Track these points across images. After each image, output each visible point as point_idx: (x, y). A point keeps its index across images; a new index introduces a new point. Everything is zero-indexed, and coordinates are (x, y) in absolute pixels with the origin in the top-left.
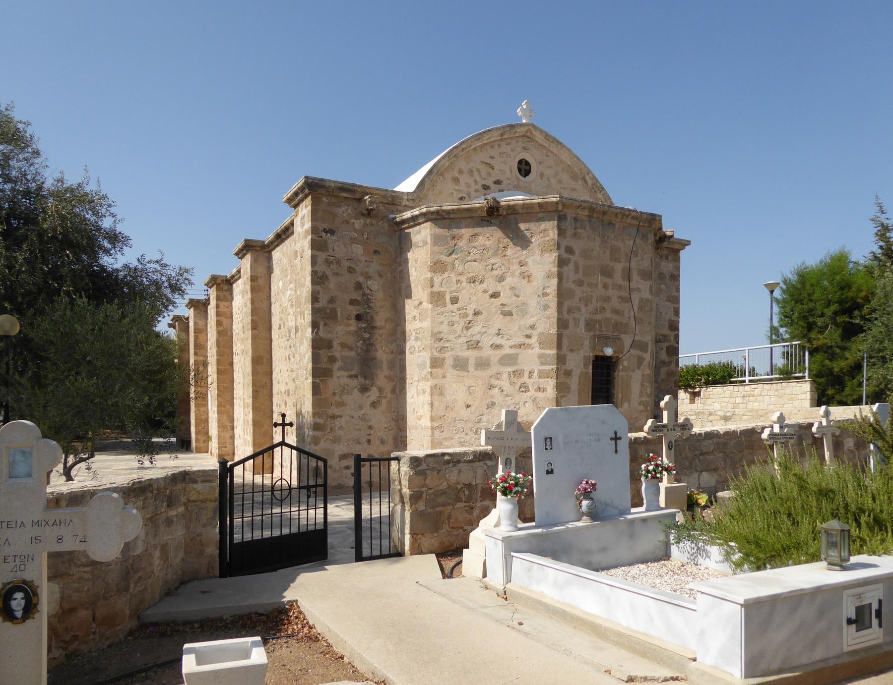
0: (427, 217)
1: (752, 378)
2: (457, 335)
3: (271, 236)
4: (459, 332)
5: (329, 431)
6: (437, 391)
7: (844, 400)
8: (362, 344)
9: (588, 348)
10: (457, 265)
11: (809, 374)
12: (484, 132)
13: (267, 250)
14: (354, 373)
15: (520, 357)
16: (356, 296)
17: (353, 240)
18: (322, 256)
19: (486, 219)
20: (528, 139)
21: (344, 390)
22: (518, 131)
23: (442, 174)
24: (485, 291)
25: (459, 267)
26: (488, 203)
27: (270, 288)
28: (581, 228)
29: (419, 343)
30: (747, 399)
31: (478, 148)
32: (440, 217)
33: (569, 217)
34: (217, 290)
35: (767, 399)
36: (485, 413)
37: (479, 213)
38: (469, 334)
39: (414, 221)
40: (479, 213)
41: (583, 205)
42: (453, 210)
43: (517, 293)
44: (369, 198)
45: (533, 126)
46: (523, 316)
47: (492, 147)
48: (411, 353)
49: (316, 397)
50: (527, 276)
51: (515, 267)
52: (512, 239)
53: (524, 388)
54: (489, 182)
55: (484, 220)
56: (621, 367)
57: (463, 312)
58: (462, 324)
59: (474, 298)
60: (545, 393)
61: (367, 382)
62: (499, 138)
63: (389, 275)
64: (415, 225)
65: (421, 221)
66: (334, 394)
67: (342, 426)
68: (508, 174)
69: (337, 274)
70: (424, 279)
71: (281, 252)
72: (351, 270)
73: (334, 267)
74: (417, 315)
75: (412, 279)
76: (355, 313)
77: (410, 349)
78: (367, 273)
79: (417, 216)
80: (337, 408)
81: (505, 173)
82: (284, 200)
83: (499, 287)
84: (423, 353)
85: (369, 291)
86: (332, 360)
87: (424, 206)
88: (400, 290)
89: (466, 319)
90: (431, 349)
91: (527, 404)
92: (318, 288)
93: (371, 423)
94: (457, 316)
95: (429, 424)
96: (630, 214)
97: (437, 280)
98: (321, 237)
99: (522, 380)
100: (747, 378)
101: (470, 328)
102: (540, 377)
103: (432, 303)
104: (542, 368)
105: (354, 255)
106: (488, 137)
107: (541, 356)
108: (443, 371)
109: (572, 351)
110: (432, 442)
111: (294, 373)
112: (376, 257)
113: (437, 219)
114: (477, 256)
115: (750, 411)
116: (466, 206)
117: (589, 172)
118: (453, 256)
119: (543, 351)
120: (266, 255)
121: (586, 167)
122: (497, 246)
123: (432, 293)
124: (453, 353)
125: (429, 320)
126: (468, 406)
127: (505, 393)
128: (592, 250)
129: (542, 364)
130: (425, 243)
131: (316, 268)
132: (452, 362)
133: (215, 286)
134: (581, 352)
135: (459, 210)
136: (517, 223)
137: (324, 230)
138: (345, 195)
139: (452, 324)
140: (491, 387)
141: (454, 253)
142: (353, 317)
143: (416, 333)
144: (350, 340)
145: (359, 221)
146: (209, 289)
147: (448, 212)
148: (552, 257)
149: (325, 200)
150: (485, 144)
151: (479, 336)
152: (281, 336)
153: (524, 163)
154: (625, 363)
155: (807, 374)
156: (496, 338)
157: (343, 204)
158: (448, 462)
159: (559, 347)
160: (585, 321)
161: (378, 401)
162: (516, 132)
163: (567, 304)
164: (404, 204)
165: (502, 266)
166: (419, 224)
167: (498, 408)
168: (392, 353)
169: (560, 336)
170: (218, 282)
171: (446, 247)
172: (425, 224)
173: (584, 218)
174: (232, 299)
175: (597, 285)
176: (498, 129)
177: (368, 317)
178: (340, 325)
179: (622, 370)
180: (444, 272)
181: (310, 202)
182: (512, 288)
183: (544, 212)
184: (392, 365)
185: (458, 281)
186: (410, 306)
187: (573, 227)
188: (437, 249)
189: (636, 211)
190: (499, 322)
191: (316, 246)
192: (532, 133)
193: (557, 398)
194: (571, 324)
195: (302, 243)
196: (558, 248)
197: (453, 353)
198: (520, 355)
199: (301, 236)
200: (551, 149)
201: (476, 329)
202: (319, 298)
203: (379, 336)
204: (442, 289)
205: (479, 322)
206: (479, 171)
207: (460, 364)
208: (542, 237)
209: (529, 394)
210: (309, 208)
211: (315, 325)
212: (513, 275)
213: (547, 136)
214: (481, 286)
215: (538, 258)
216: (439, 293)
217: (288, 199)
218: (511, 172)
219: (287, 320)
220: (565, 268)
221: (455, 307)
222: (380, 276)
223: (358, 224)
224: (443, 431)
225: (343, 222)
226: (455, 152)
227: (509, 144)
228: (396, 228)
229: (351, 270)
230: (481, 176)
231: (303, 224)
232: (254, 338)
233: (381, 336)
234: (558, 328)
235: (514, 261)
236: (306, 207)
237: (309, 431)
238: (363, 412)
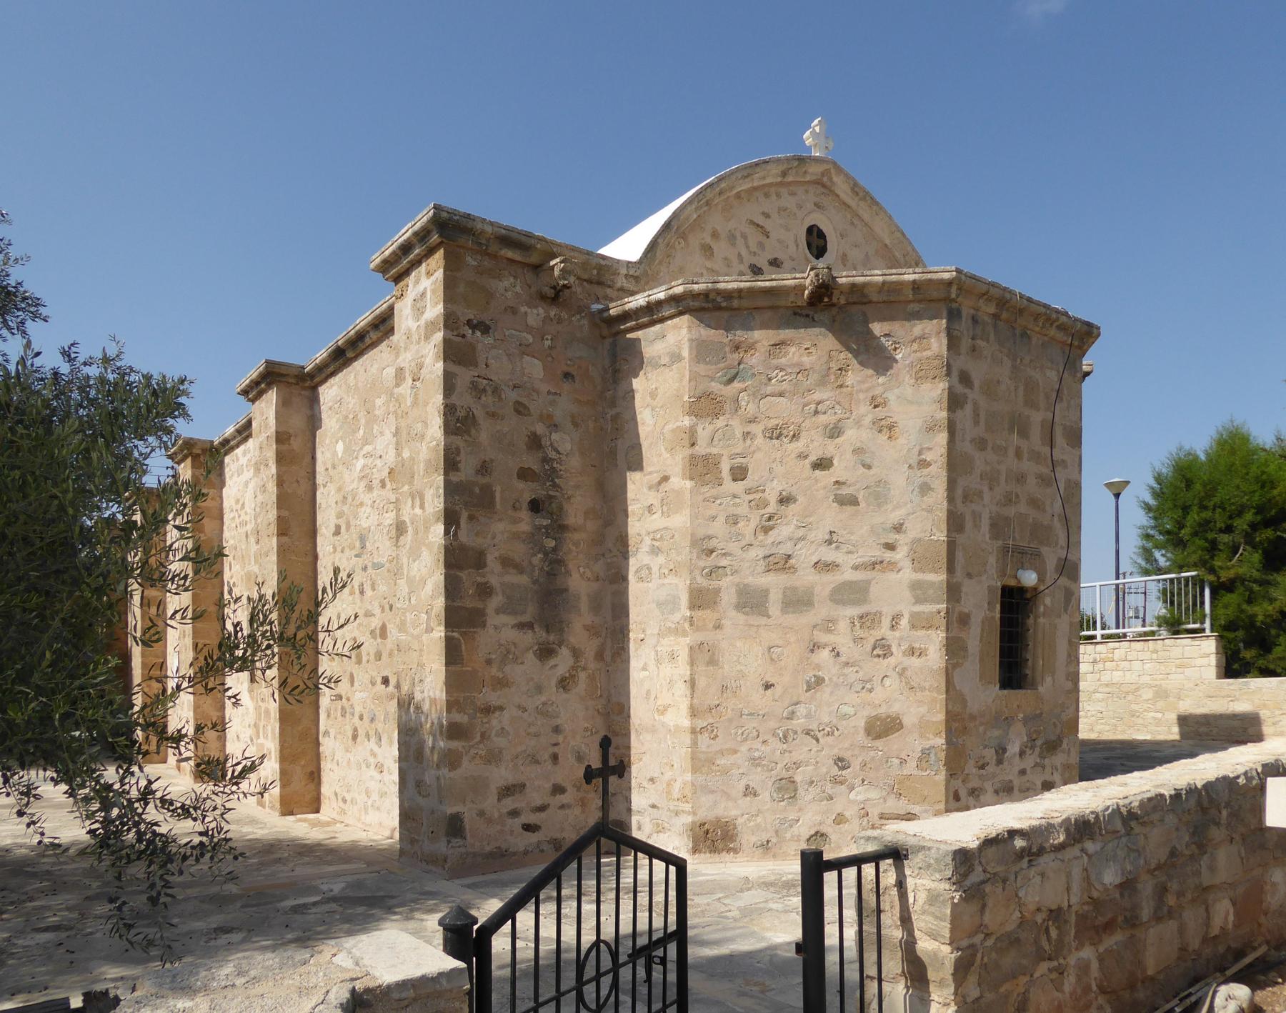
0: (682, 305)
1: (1107, 632)
2: (744, 543)
3: (321, 355)
4: (749, 537)
5: (478, 738)
6: (703, 655)
7: (1272, 667)
8: (541, 560)
9: (994, 571)
10: (743, 403)
11: (1212, 625)
12: (757, 164)
13: (307, 384)
14: (526, 618)
15: (874, 589)
16: (531, 461)
17: (525, 350)
18: (465, 376)
19: (804, 312)
20: (823, 190)
21: (509, 655)
22: (811, 170)
23: (684, 236)
24: (802, 456)
25: (748, 406)
26: (817, 275)
27: (314, 458)
28: (982, 339)
29: (661, 559)
30: (1101, 666)
31: (743, 195)
32: (710, 305)
33: (964, 313)
34: (193, 467)
35: (1137, 665)
36: (802, 699)
37: (792, 298)
38: (770, 540)
39: (652, 313)
40: (792, 298)
41: (993, 291)
42: (740, 291)
43: (868, 461)
44: (561, 262)
45: (835, 164)
46: (879, 506)
47: (767, 195)
48: (641, 579)
49: (452, 668)
50: (887, 428)
51: (864, 409)
52: (856, 354)
53: (882, 649)
54: (762, 262)
55: (800, 315)
56: (1042, 609)
57: (757, 496)
58: (754, 522)
59: (779, 469)
60: (923, 659)
61: (552, 638)
62: (779, 179)
63: (591, 424)
64: (652, 323)
65: (667, 314)
66: (489, 662)
67: (503, 728)
68: (792, 248)
69: (493, 415)
70: (673, 431)
71: (340, 387)
72: (520, 409)
73: (488, 399)
74: (656, 503)
75: (643, 431)
76: (527, 497)
77: (637, 571)
78: (550, 416)
79: (659, 303)
80: (493, 690)
81: (787, 247)
82: (372, 266)
83: (830, 448)
84: (672, 580)
85: (554, 453)
86: (485, 591)
87: (680, 282)
88: (613, 453)
89: (763, 512)
90: (691, 572)
91: (887, 682)
92: (458, 441)
93: (559, 721)
94: (746, 505)
95: (686, 723)
96: (1058, 319)
97: (704, 431)
98: (464, 336)
99: (877, 634)
100: (1099, 632)
101: (771, 528)
102: (913, 627)
103: (692, 479)
104: (918, 608)
105: (526, 379)
106: (761, 174)
107: (915, 586)
108: (715, 615)
109: (969, 575)
110: (692, 759)
111: (372, 619)
112: (566, 386)
113: (703, 309)
114: (785, 385)
115: (1107, 685)
116: (767, 284)
118: (737, 385)
119: (920, 576)
120: (306, 393)
121: (914, 250)
122: (825, 367)
123: (692, 457)
124: (736, 578)
125: (687, 512)
126: (768, 686)
127: (843, 659)
128: (998, 382)
129: (918, 601)
130: (676, 358)
131: (454, 399)
132: (735, 596)
133: (189, 461)
134: (984, 578)
135: (752, 292)
136: (866, 322)
137: (469, 322)
138: (509, 254)
139: (733, 520)
140: (815, 647)
141: (738, 379)
142: (525, 505)
143: (653, 539)
144: (519, 551)
145: (535, 311)
146: (175, 466)
147: (728, 295)
148: (937, 389)
149: (470, 261)
150: (755, 189)
151: (790, 544)
152: (339, 549)
153: (815, 234)
154: (1048, 601)
155: (1207, 625)
156: (824, 549)
157: (506, 273)
158: (1022, 854)
159: (951, 569)
160: (991, 518)
161: (572, 676)
162: (805, 172)
163: (962, 483)
164: (619, 285)
165: (837, 407)
166: (662, 320)
167: (828, 690)
168: (597, 579)
169: (951, 546)
170: (197, 451)
171: (722, 365)
172: (676, 320)
173: (986, 318)
174: (223, 484)
175: (1006, 449)
176: (778, 160)
177: (554, 505)
178: (500, 520)
179: (1044, 614)
180: (716, 415)
181: (442, 263)
182: (858, 451)
183: (920, 301)
184: (596, 606)
185: (746, 435)
186: (637, 487)
187: (971, 334)
188: (702, 369)
189: (1066, 314)
190: (830, 517)
191: (455, 354)
192: (831, 179)
193: (947, 668)
194: (969, 524)
195: (418, 351)
196: (948, 374)
197: (736, 578)
198: (873, 582)
199: (415, 337)
200: (861, 212)
201: (784, 531)
202: (460, 462)
203: (574, 544)
204: (714, 451)
205: (790, 517)
206: (744, 237)
207: (752, 602)
208: (915, 352)
209: (891, 661)
210: (439, 274)
211: (450, 518)
212: (858, 423)
213: (855, 188)
214: (794, 445)
215: (909, 391)
216: (706, 458)
217: (385, 262)
218: (797, 246)
219: (356, 516)
220: (959, 413)
221: (741, 485)
222: (576, 425)
223: (535, 315)
224: (717, 736)
225: (506, 309)
226: (709, 195)
227: (793, 194)
228: (605, 332)
229: (520, 409)
230: (748, 247)
231: (418, 311)
232: (282, 552)
233: (577, 544)
234: (948, 530)
235: (862, 396)
236: (429, 274)
237: (434, 740)
238: (543, 699)
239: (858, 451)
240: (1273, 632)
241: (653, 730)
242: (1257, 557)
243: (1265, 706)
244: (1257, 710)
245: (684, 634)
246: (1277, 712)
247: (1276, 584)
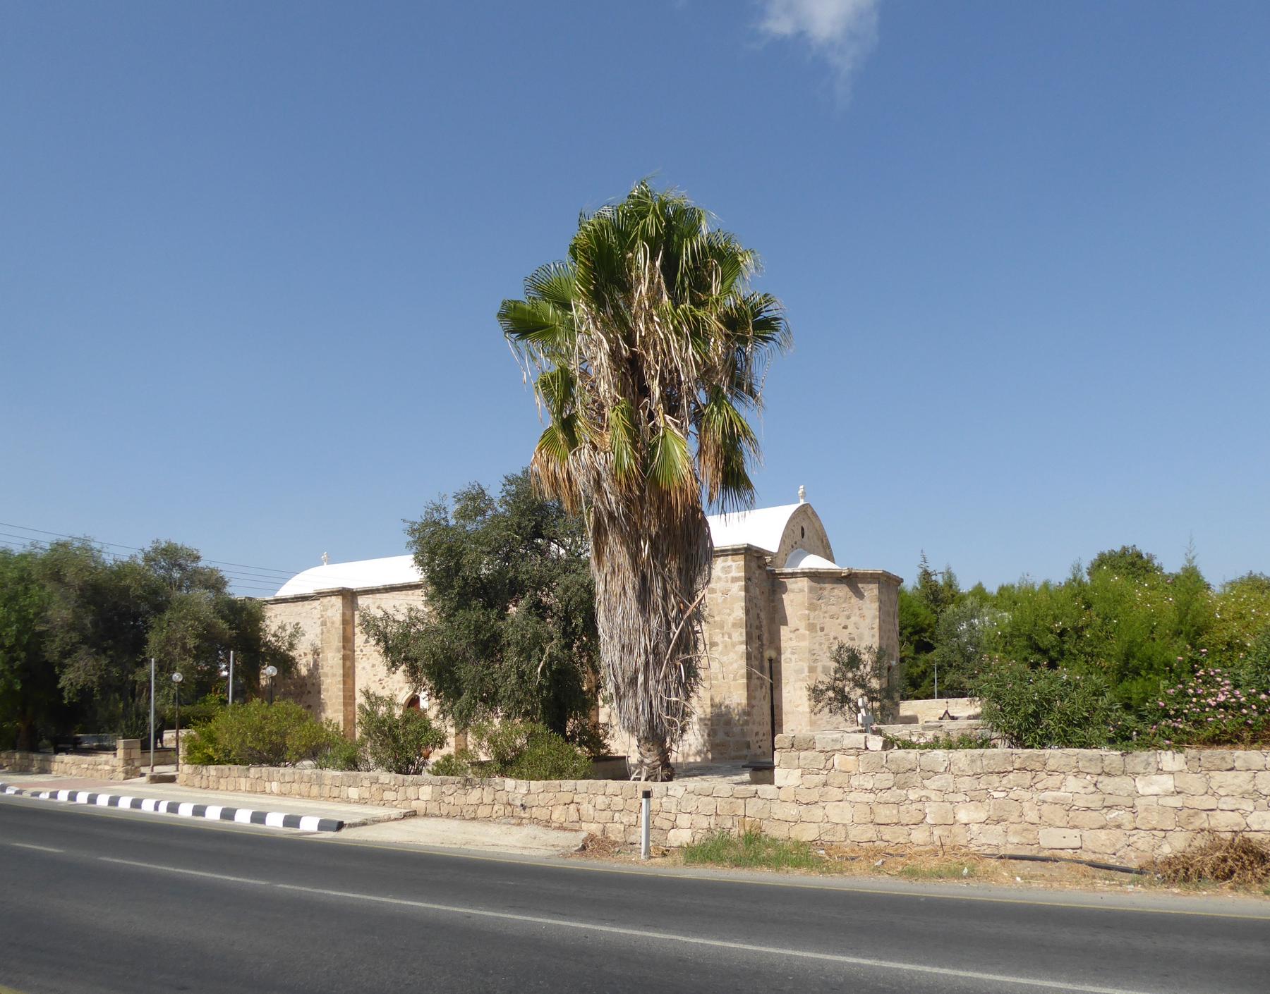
29: (796, 656)
50: (862, 616)
83: (847, 622)
117: (826, 536)
139: (821, 644)
148: (876, 605)
180: (816, 610)
185: (824, 617)
186: (784, 631)
204: (815, 622)
212: (855, 615)
239: (855, 624)
240: (919, 680)
242: (912, 648)
245: (806, 681)
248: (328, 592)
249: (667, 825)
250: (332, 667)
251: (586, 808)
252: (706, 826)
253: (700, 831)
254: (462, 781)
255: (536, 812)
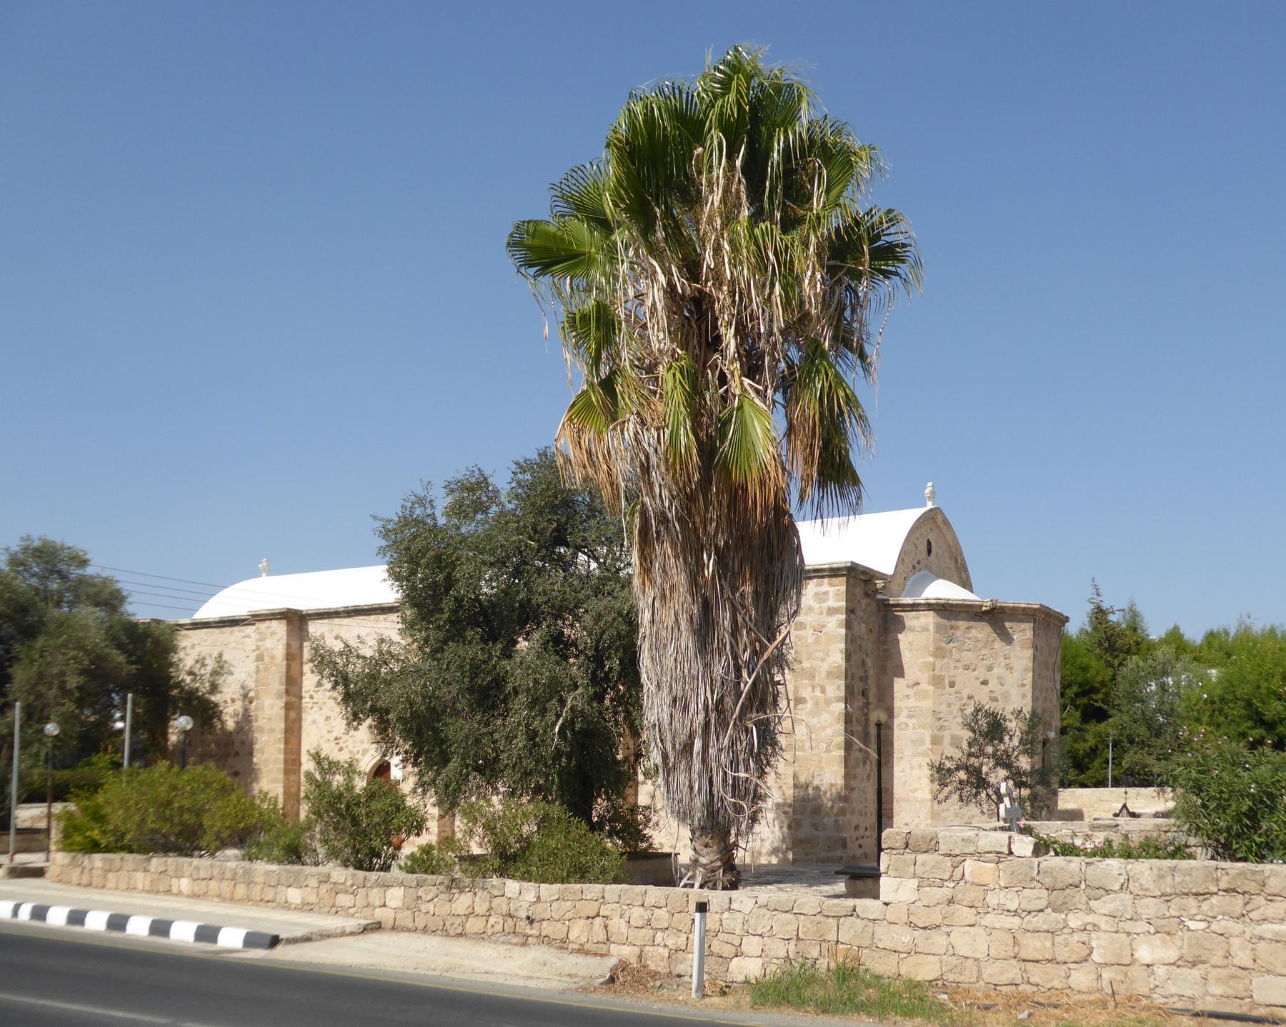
4: (955, 714)
7: (1086, 782)
29: (914, 720)
48: (901, 729)
51: (1002, 659)
79: (920, 604)
83: (988, 676)
97: (939, 664)
123: (933, 675)
124: (950, 732)
136: (1003, 622)
139: (949, 705)
148: (1029, 653)
172: (926, 612)
185: (955, 667)
186: (899, 685)
188: (938, 636)
197: (950, 732)
204: (943, 673)
228: (882, 609)
240: (1086, 760)
241: (907, 800)
242: (1078, 714)
243: (1084, 805)
244: (1080, 808)
246: (1091, 809)
247: (1087, 731)
248: (267, 615)
249: (728, 951)
250: (270, 719)
251: (617, 924)
252: (782, 954)
253: (774, 961)
254: (447, 882)
255: (547, 928)
